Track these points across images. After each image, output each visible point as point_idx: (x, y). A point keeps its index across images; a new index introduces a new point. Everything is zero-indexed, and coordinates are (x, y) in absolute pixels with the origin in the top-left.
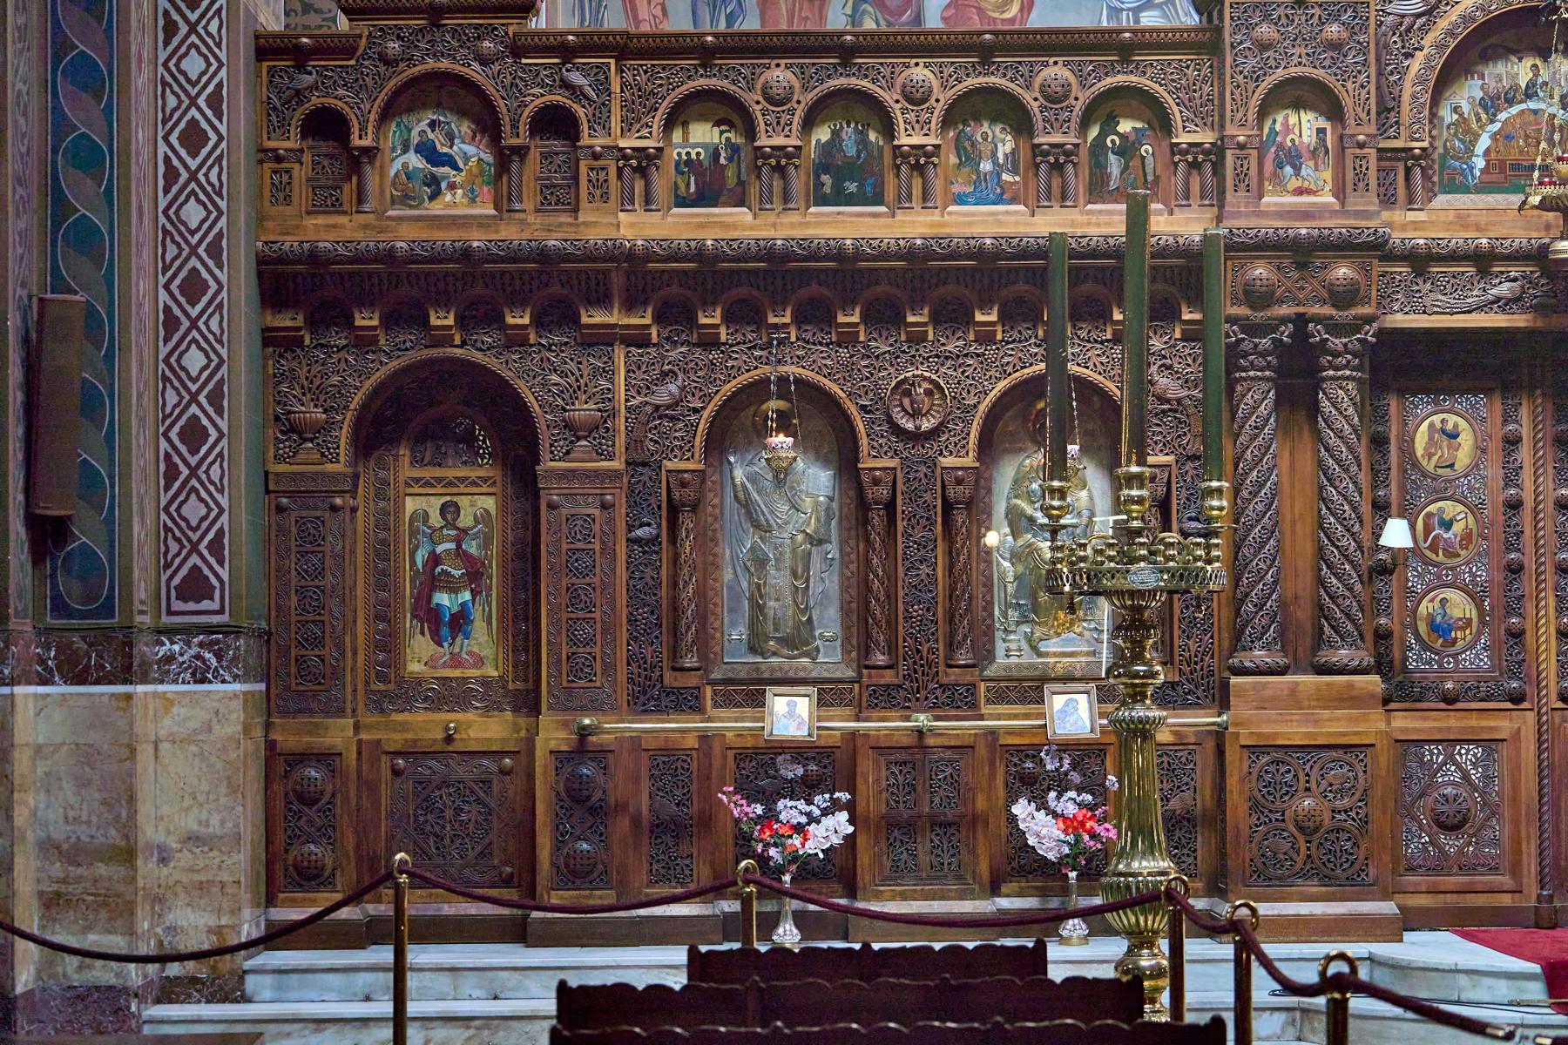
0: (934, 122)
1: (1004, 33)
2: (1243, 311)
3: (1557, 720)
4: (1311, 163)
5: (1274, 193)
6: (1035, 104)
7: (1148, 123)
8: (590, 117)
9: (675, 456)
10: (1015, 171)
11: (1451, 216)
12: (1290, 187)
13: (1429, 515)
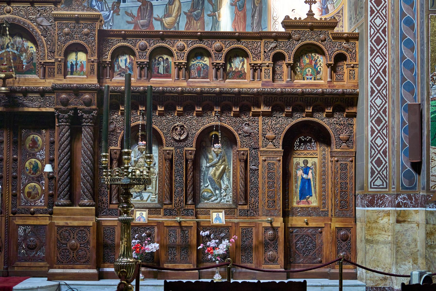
0: (185, 56)
8: (351, 56)
9: (113, 145)
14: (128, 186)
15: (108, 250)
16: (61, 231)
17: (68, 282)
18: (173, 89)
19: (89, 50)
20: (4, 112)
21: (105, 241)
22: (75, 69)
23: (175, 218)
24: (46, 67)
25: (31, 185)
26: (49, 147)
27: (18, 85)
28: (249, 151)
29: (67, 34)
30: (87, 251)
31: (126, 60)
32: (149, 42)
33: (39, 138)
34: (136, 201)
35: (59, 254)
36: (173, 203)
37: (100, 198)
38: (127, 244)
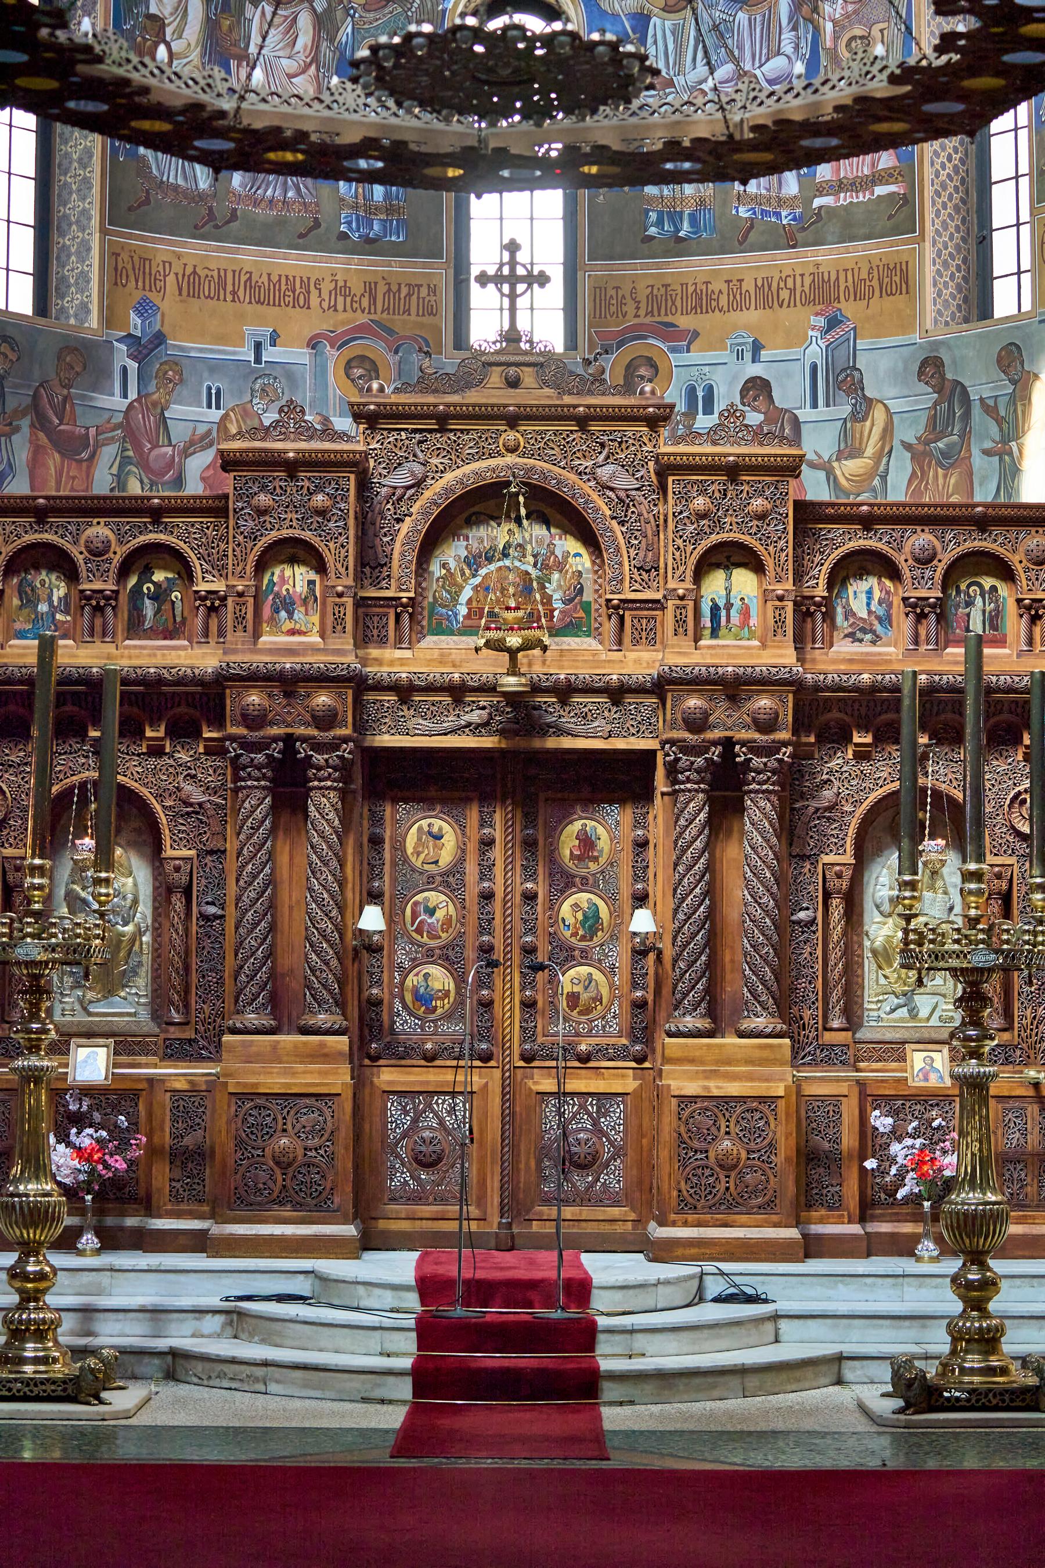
1: (54, 498)
2: (241, 731)
3: (519, 1077)
4: (302, 609)
5: (271, 633)
6: (81, 557)
7: (179, 574)
10: (67, 612)
11: (436, 653)
12: (285, 628)
13: (416, 904)
14: (982, 975)
15: (821, 1170)
16: (688, 1111)
17: (727, 1267)
18: (1017, 679)
19: (769, 563)
20: (501, 751)
21: (810, 1144)
22: (723, 619)
23: (1021, 1072)
24: (627, 613)
25: (578, 973)
26: (477, 856)
27: (545, 670)
28: (195, 860)
29: (703, 516)
30: (769, 1172)
31: (869, 593)
32: (941, 539)
33: (601, 830)
34: (895, 1021)
35: (683, 1183)
36: (1016, 1025)
37: (795, 1010)
38: (980, 1150)
